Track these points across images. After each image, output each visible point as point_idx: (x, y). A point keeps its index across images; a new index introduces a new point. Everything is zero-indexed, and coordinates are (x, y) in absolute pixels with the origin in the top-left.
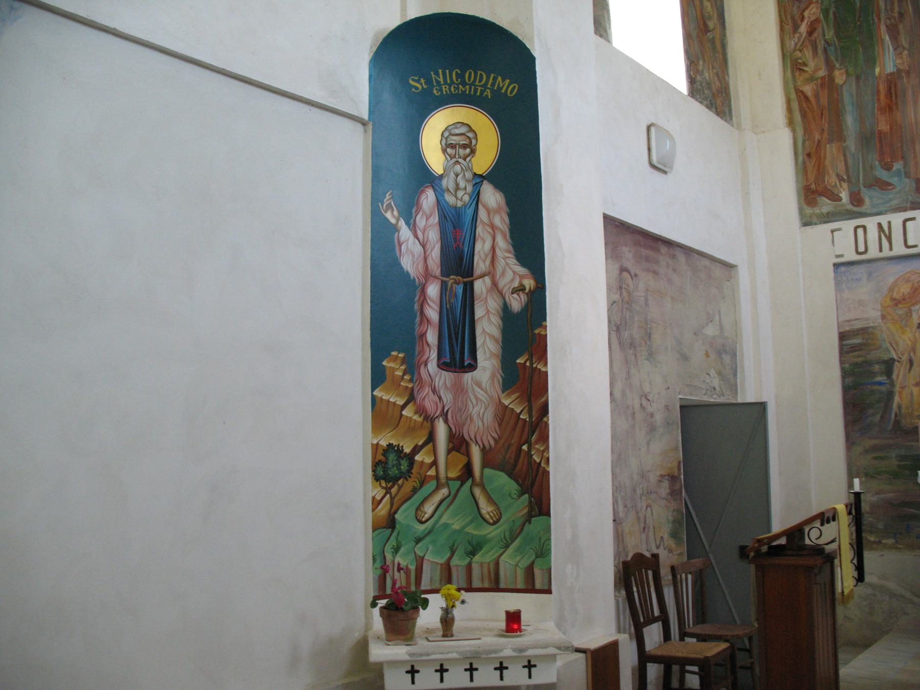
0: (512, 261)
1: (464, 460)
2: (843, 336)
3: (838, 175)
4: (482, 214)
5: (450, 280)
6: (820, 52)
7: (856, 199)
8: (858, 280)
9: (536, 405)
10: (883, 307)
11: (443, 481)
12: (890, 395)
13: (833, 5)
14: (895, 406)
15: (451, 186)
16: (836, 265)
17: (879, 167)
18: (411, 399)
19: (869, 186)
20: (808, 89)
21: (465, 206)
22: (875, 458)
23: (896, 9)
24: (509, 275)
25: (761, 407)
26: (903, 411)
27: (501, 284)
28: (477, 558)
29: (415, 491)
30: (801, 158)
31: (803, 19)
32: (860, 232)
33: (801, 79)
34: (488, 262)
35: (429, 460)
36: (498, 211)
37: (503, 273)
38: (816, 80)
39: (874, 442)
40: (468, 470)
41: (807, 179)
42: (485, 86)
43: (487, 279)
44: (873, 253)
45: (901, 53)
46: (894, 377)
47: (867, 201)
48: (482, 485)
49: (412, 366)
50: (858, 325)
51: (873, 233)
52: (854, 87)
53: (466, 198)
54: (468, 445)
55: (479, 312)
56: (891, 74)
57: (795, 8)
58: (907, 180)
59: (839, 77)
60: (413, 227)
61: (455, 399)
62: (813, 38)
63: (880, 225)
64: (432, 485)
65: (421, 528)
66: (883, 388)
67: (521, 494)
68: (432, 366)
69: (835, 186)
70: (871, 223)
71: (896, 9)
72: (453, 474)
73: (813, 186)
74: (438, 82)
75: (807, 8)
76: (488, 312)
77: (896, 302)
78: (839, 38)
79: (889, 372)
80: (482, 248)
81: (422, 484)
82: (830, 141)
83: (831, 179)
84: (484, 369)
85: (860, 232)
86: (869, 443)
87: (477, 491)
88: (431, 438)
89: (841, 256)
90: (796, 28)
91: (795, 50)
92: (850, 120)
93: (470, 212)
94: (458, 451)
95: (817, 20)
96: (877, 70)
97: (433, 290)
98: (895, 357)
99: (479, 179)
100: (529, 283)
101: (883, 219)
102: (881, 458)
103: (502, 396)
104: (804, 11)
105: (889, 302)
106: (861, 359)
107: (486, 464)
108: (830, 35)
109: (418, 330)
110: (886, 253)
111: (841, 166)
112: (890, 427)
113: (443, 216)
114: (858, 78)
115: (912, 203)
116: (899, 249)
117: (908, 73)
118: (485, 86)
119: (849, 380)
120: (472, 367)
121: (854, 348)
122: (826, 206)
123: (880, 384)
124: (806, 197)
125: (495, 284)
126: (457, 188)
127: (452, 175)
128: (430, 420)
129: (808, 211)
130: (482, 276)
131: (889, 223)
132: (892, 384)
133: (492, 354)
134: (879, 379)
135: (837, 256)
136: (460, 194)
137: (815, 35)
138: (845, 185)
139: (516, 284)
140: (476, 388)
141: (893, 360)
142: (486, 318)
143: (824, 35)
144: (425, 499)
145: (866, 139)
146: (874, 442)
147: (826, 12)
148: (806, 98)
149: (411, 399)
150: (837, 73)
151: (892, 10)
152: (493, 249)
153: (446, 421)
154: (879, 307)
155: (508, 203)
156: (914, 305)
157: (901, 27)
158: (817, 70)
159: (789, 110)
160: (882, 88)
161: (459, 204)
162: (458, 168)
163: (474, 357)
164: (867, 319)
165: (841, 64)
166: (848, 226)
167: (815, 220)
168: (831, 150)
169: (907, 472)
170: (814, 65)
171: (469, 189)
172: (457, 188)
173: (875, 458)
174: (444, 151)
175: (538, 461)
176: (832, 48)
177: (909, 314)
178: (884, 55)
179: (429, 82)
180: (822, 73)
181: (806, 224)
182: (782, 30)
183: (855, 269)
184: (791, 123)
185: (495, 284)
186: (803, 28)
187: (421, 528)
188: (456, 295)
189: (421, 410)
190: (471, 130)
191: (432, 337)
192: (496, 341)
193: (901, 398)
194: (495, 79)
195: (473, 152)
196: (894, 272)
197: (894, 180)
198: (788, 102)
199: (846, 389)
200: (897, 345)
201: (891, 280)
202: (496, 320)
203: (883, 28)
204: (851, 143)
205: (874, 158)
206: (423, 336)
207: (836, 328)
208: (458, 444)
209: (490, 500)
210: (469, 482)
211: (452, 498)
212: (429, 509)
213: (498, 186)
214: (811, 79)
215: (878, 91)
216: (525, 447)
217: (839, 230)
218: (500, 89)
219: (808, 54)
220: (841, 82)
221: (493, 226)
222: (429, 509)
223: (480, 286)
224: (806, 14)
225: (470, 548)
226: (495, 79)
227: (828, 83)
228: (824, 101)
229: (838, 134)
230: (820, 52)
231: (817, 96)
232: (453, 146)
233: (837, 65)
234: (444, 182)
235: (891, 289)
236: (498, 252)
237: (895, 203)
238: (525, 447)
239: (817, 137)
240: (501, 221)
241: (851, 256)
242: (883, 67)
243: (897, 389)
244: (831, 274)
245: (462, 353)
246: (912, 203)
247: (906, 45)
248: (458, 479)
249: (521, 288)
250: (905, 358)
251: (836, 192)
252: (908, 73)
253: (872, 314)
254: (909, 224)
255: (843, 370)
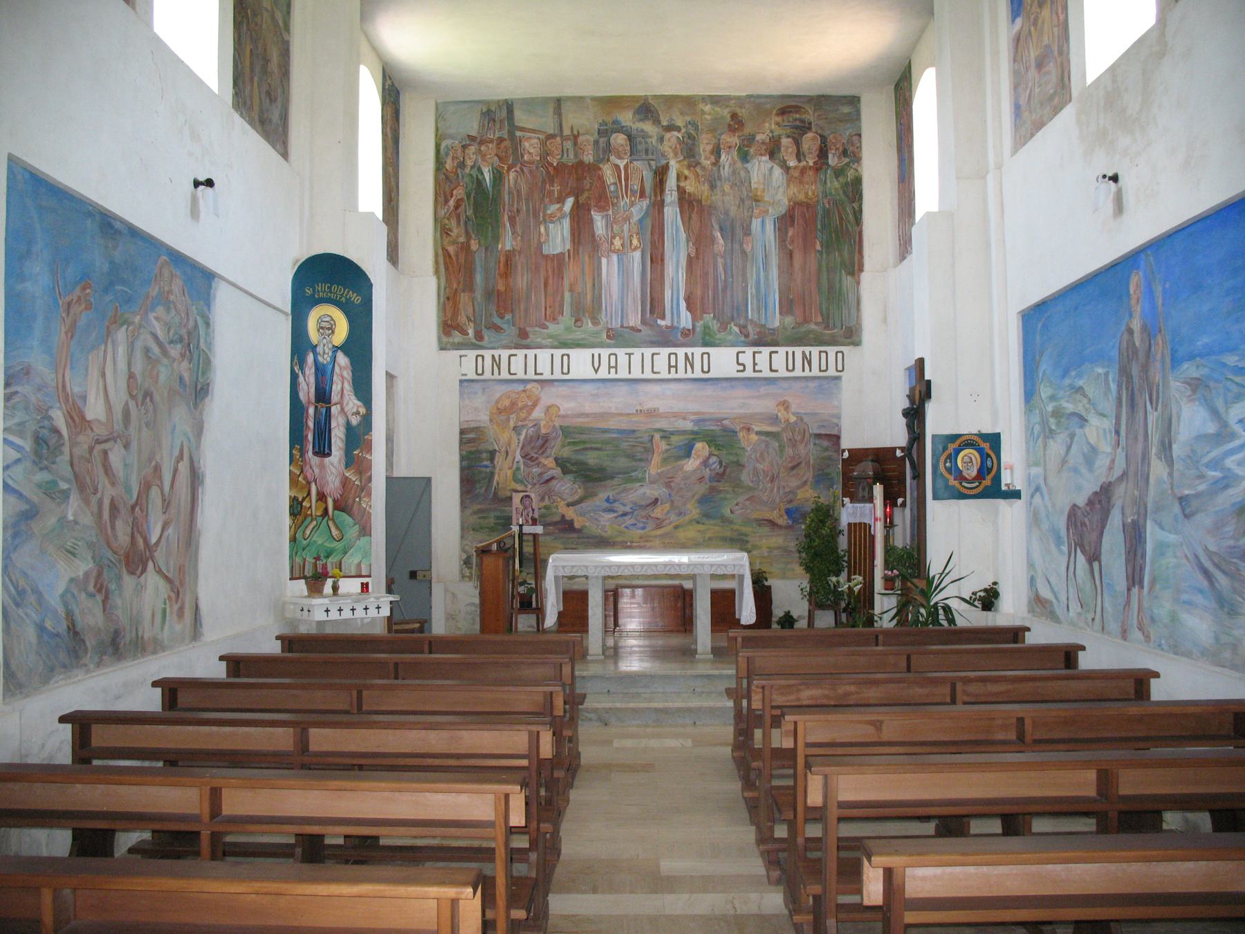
0: (353, 397)
1: (324, 506)
2: (462, 432)
3: (468, 317)
4: (337, 369)
5: (319, 405)
6: (462, 223)
7: (479, 336)
8: (476, 393)
9: (364, 478)
10: (491, 413)
11: (314, 517)
12: (492, 474)
13: (474, 191)
14: (495, 483)
15: (321, 353)
16: (461, 381)
17: (495, 316)
18: (302, 471)
19: (488, 328)
20: (451, 249)
21: (327, 363)
22: (480, 518)
23: (515, 206)
24: (351, 405)
25: (1020, 491)
26: (500, 485)
27: (346, 410)
28: (330, 559)
29: (303, 522)
30: (442, 299)
31: (452, 196)
32: (480, 359)
33: (447, 240)
34: (339, 397)
35: (308, 505)
36: (345, 368)
37: (348, 404)
38: (458, 243)
39: (479, 507)
40: (326, 511)
41: (445, 316)
42: (342, 295)
43: (338, 406)
44: (487, 375)
45: (516, 238)
46: (496, 462)
47: (486, 338)
48: (333, 520)
49: (303, 452)
50: (473, 425)
51: (488, 361)
52: (483, 255)
53: (329, 359)
54: (326, 497)
55: (333, 424)
56: (509, 251)
57: (447, 186)
58: (513, 328)
59: (474, 246)
60: (304, 374)
61: (320, 472)
62: (458, 212)
63: (493, 356)
64: (309, 519)
65: (305, 542)
66: (488, 470)
67: (355, 524)
68: (310, 453)
69: (465, 324)
70: (488, 354)
71: (515, 206)
72: (319, 514)
73: (449, 322)
74: (318, 291)
75: (455, 188)
76: (338, 425)
77: (500, 411)
78: (476, 217)
79: (492, 459)
80: (336, 388)
81: (305, 518)
82: (464, 291)
83: (462, 319)
84: (335, 456)
85: (480, 359)
86: (476, 507)
87: (331, 523)
88: (309, 494)
89: (465, 375)
90: (446, 201)
91: (444, 218)
92: (479, 278)
93: (330, 367)
94: (321, 500)
95: (461, 200)
96: (500, 246)
97: (311, 411)
98: (497, 449)
99: (336, 349)
100: (363, 410)
101: (496, 353)
102: (483, 517)
103: (345, 471)
104: (453, 190)
105: (495, 411)
106: (474, 449)
107: (336, 508)
108: (470, 212)
109: (305, 434)
110: (496, 376)
111: (470, 310)
112: (491, 496)
113: (317, 369)
114: (487, 249)
115: (515, 344)
116: (505, 375)
117: (520, 252)
118: (342, 295)
119: (465, 463)
120: (329, 455)
121: (470, 441)
122: (457, 337)
123: (486, 467)
124: (444, 329)
125: (342, 409)
126: (324, 353)
127: (322, 345)
128: (309, 483)
129: (445, 339)
130: (336, 404)
131: (500, 356)
132: (494, 467)
133: (340, 448)
134: (486, 463)
135: (463, 375)
136: (326, 356)
137: (460, 210)
138: (472, 324)
139: (355, 410)
140: (331, 467)
141: (495, 451)
142: (337, 429)
143: (466, 212)
144: (306, 527)
145: (489, 294)
146: (479, 507)
147: (468, 196)
148: (450, 256)
149: (302, 471)
150: (472, 242)
151: (513, 205)
152: (342, 389)
153: (316, 484)
154: (488, 413)
155: (351, 364)
156: (512, 414)
157: (517, 219)
158: (458, 236)
159: (437, 262)
160: (502, 259)
161: (325, 362)
162: (325, 341)
163: (331, 450)
164: (479, 421)
165: (476, 236)
166: (472, 354)
167: (449, 346)
168: (464, 298)
169: (500, 528)
170: (457, 231)
171: (330, 354)
172: (324, 353)
173: (480, 518)
174: (318, 331)
175: (365, 506)
176: (471, 223)
177: (508, 420)
178: (505, 236)
179: (314, 290)
180: (462, 239)
181: (443, 348)
182: (436, 201)
183: (473, 385)
184: (437, 272)
185: (342, 409)
186: (452, 203)
187: (305, 542)
188: (322, 414)
189: (305, 478)
190: (332, 319)
191: (310, 437)
192: (343, 441)
193: (499, 476)
194: (348, 292)
195: (333, 332)
196: (500, 390)
197: (505, 326)
198: (436, 255)
199: (462, 469)
200: (499, 440)
201: (498, 395)
202: (343, 429)
203: (506, 218)
204: (479, 295)
205: (493, 308)
206: (307, 436)
207: (458, 424)
208: (322, 497)
209: (337, 527)
210: (326, 518)
211: (318, 526)
212: (308, 532)
213: (346, 353)
214: (454, 242)
215: (499, 262)
216: (357, 499)
217: (466, 356)
218: (350, 298)
219: (453, 223)
220: (475, 250)
221: (343, 377)
222: (308, 532)
223: (334, 410)
224: (455, 192)
225: (326, 554)
226: (348, 292)
227: (465, 247)
228: (462, 260)
229: (469, 287)
230: (462, 223)
231: (457, 256)
232: (322, 328)
233: (473, 236)
234: (318, 349)
235: (497, 402)
236: (345, 391)
237: (504, 342)
238: (357, 499)
239: (455, 286)
240: (347, 374)
241: (472, 376)
242: (504, 245)
243: (497, 471)
244: (457, 387)
245: (324, 447)
246: (515, 344)
247: (520, 233)
248: (321, 516)
249: (358, 413)
250: (503, 449)
251: (465, 328)
252: (520, 252)
253: (483, 418)
254: (512, 358)
255: (461, 455)
